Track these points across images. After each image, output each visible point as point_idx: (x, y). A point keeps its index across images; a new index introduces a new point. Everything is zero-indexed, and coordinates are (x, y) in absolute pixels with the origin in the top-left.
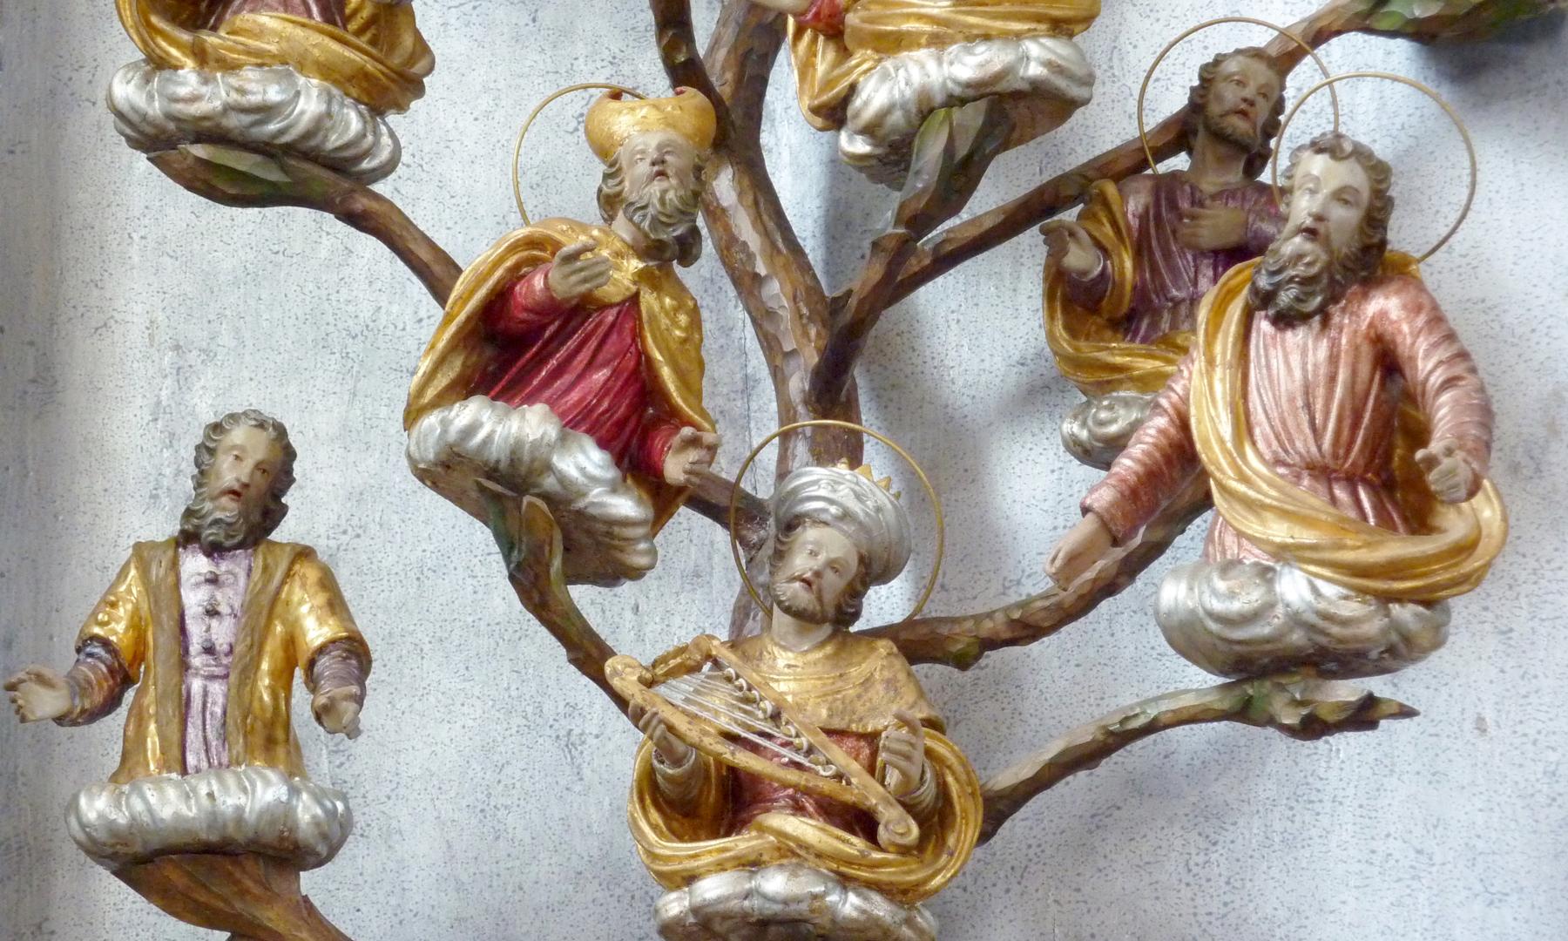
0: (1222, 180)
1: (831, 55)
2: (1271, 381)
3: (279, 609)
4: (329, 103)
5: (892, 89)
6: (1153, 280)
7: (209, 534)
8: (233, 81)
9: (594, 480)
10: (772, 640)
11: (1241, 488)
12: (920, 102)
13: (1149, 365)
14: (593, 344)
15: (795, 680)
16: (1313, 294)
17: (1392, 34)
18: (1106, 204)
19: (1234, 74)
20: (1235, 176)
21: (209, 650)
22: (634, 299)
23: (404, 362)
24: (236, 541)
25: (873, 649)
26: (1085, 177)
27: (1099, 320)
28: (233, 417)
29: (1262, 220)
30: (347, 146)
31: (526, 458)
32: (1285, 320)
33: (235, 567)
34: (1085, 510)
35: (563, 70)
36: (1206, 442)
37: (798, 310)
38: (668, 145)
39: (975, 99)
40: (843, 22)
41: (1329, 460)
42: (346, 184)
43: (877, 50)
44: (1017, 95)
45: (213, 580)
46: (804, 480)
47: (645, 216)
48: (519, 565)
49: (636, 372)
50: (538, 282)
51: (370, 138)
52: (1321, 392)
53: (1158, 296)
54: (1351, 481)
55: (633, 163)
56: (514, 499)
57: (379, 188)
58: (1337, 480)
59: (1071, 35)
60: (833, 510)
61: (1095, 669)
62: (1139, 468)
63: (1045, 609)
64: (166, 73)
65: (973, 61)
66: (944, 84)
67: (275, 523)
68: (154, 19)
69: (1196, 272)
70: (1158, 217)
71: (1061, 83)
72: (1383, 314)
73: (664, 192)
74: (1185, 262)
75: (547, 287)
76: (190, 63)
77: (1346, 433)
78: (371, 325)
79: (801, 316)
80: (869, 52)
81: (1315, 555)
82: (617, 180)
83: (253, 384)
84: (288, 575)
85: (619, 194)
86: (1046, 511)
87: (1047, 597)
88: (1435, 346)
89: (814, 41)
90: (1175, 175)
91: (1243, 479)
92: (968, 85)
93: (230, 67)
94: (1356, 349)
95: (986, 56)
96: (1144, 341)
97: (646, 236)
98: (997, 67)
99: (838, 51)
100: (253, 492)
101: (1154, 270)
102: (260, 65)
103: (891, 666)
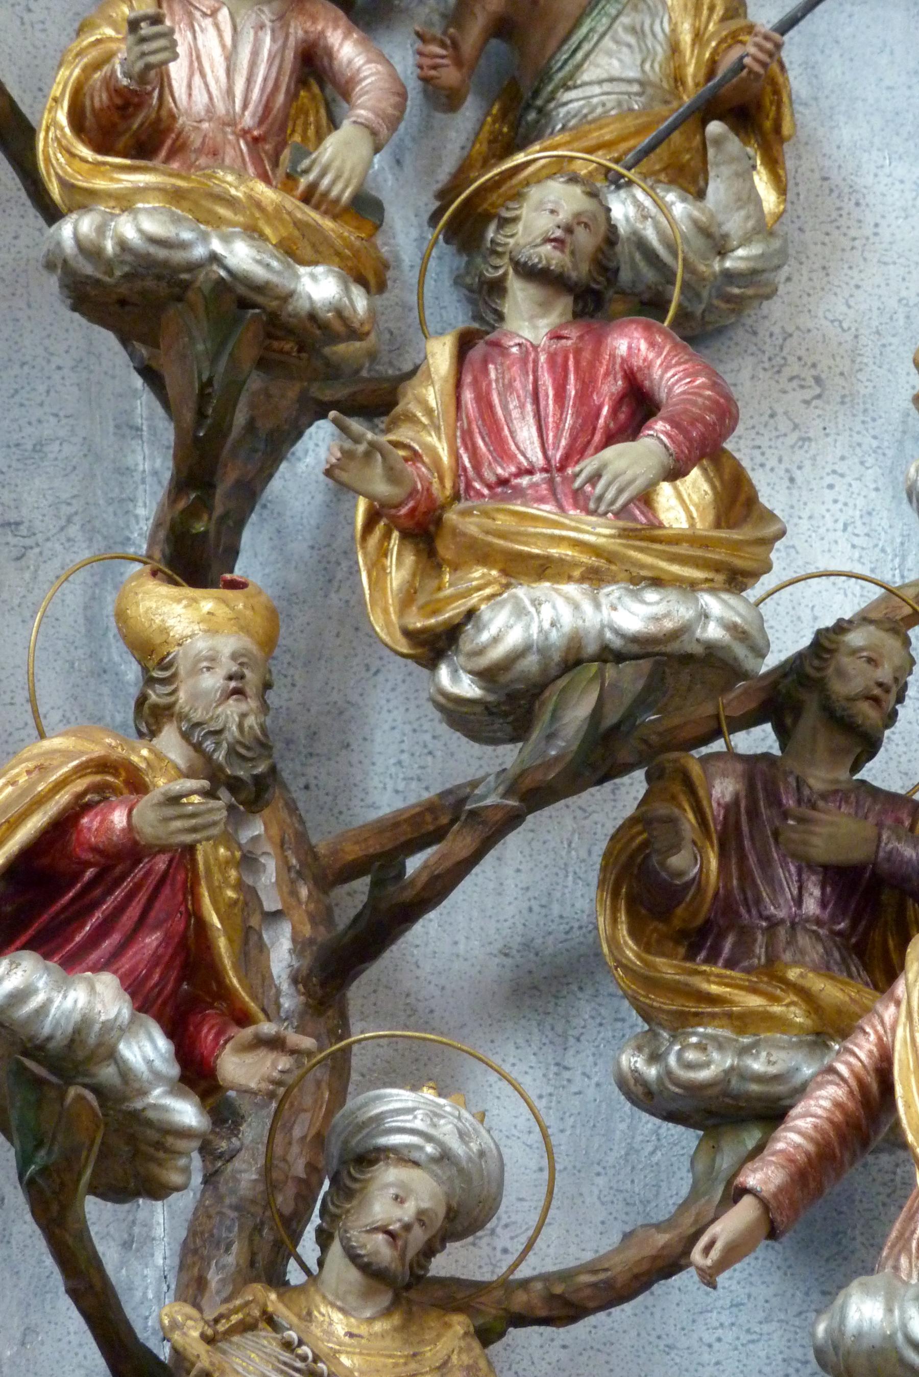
0: (830, 776)
1: (410, 559)
5: (528, 627)
6: (743, 890)
9: (158, 1076)
10: (324, 1297)
12: (568, 649)
13: (754, 1002)
15: (361, 1354)
19: (862, 649)
25: (448, 1326)
29: (899, 840)
31: (92, 1040)
38: (243, 655)
39: (636, 657)
40: (439, 522)
43: (504, 572)
44: (687, 659)
47: (218, 744)
48: (44, 1171)
50: (119, 818)
53: (749, 911)
55: (195, 671)
56: (58, 1087)
60: (429, 1149)
61: (586, 1354)
63: (594, 1285)
65: (644, 611)
66: (601, 633)
69: (800, 888)
70: (753, 814)
71: (741, 651)
73: (243, 716)
75: (130, 827)
79: (290, 869)
80: (494, 573)
82: (169, 689)
85: (170, 707)
86: (530, 1147)
87: (595, 1272)
89: (387, 536)
92: (635, 639)
96: (730, 964)
99: (418, 553)
101: (745, 876)
103: (469, 1349)
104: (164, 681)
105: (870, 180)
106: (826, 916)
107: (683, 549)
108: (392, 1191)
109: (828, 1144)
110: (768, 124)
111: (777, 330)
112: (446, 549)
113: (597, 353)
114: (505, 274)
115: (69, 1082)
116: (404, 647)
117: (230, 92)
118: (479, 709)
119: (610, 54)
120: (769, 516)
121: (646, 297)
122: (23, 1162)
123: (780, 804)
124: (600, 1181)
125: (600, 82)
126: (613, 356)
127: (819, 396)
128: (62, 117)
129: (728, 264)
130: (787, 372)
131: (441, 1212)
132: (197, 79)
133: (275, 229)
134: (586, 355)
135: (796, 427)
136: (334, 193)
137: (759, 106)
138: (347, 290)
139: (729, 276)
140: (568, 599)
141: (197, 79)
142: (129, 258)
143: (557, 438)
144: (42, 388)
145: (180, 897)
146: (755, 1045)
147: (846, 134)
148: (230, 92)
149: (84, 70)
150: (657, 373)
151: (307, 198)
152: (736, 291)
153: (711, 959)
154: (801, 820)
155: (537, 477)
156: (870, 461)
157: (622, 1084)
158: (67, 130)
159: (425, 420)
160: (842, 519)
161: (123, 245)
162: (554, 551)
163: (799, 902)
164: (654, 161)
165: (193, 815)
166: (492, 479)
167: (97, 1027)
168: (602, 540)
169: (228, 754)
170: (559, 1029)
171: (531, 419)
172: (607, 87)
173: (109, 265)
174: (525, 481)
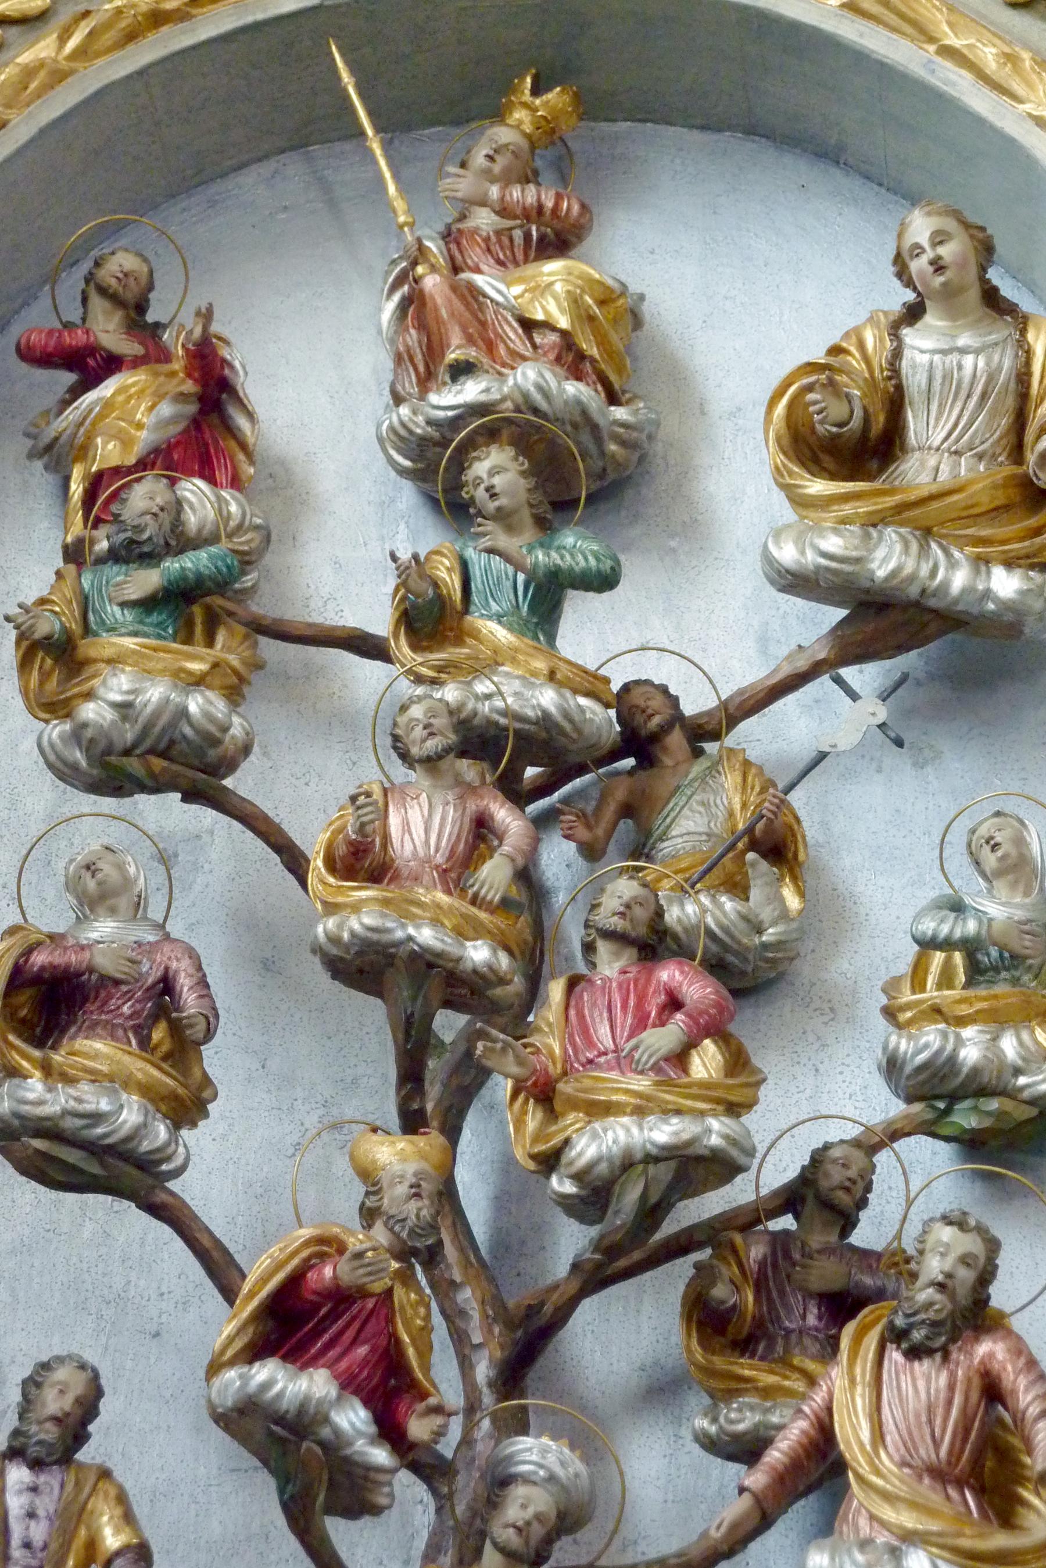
1: (539, 1115)
2: (901, 1400)
3: (85, 1516)
4: (146, 1115)
5: (600, 1146)
7: (33, 1451)
8: (71, 1091)
9: (360, 1434)
11: (879, 1482)
12: (624, 1157)
13: (771, 1379)
14: (356, 1325)
16: (940, 1334)
17: (947, 1139)
18: (734, 1250)
20: (833, 1238)
21: (27, 1545)
22: (389, 1292)
23: (147, 1327)
24: (55, 1458)
26: (713, 1228)
27: (722, 1340)
28: (60, 1360)
29: (862, 1273)
30: (158, 1150)
31: (312, 1411)
32: (914, 1353)
33: (51, 1479)
34: (742, 1490)
35: (285, 1108)
36: (848, 1443)
37: (485, 1311)
39: (667, 1159)
40: (554, 1090)
41: (944, 1465)
42: (150, 1181)
43: (588, 1114)
44: (699, 1159)
45: (34, 1489)
46: (520, 1447)
47: (403, 1227)
48: (292, 1497)
49: (387, 1351)
50: (328, 1272)
51: (173, 1145)
52: (940, 1411)
54: (960, 1484)
55: (392, 1185)
57: (173, 1185)
58: (950, 1482)
59: (738, 1116)
60: (542, 1473)
62: (785, 1460)
64: (16, 1081)
66: (644, 1146)
67: (81, 1445)
68: (11, 1037)
70: (775, 1265)
71: (734, 1153)
72: (991, 1355)
73: (419, 1209)
74: (796, 1300)
75: (335, 1277)
76: (38, 1074)
77: (958, 1444)
78: (123, 1294)
81: (940, 1540)
83: (24, 1333)
84: (94, 1489)
85: (379, 1208)
88: (1033, 1383)
89: (526, 1101)
90: (786, 1232)
91: (878, 1473)
92: (663, 1148)
93: (69, 1080)
94: (969, 1380)
95: (680, 1126)
96: (762, 1358)
97: (405, 1242)
98: (686, 1136)
99: (545, 1111)
100: (71, 1420)
102: (94, 1081)
104: (374, 1193)
105: (861, 888)
106: (822, 1325)
107: (694, 1091)
108: (520, 1501)
109: (799, 1456)
110: (790, 855)
111: (805, 981)
112: (558, 1106)
113: (648, 981)
114: (594, 939)
115: (303, 1438)
116: (531, 1165)
117: (427, 842)
118: (577, 1201)
119: (687, 818)
120: (757, 1071)
121: (714, 962)
122: (281, 1492)
123: (791, 1258)
124: (703, 1507)
125: (681, 836)
126: (659, 982)
127: (833, 1019)
128: (320, 863)
129: (764, 938)
130: (813, 1006)
131: (553, 1515)
132: (407, 836)
133: (450, 919)
134: (642, 981)
135: (819, 1038)
136: (489, 898)
137: (785, 846)
138: (494, 952)
139: (765, 946)
140: (623, 1126)
141: (407, 836)
142: (355, 941)
143: (622, 1031)
144: (357, 1046)
145: (383, 1324)
146: (774, 1407)
147: (847, 861)
148: (427, 842)
149: (333, 833)
150: (685, 988)
151: (474, 902)
152: (771, 955)
153: (752, 1356)
154: (804, 1266)
155: (610, 1056)
156: (865, 1056)
157: (697, 1439)
158: (323, 870)
159: (546, 1029)
160: (849, 1091)
161: (353, 934)
162: (614, 1098)
163: (804, 1317)
164: (710, 879)
165: (369, 1265)
166: (584, 1060)
167: (314, 1402)
168: (641, 1088)
169: (409, 1235)
170: (676, 1414)
171: (606, 1023)
172: (686, 838)
173: (347, 947)
174: (602, 1059)
